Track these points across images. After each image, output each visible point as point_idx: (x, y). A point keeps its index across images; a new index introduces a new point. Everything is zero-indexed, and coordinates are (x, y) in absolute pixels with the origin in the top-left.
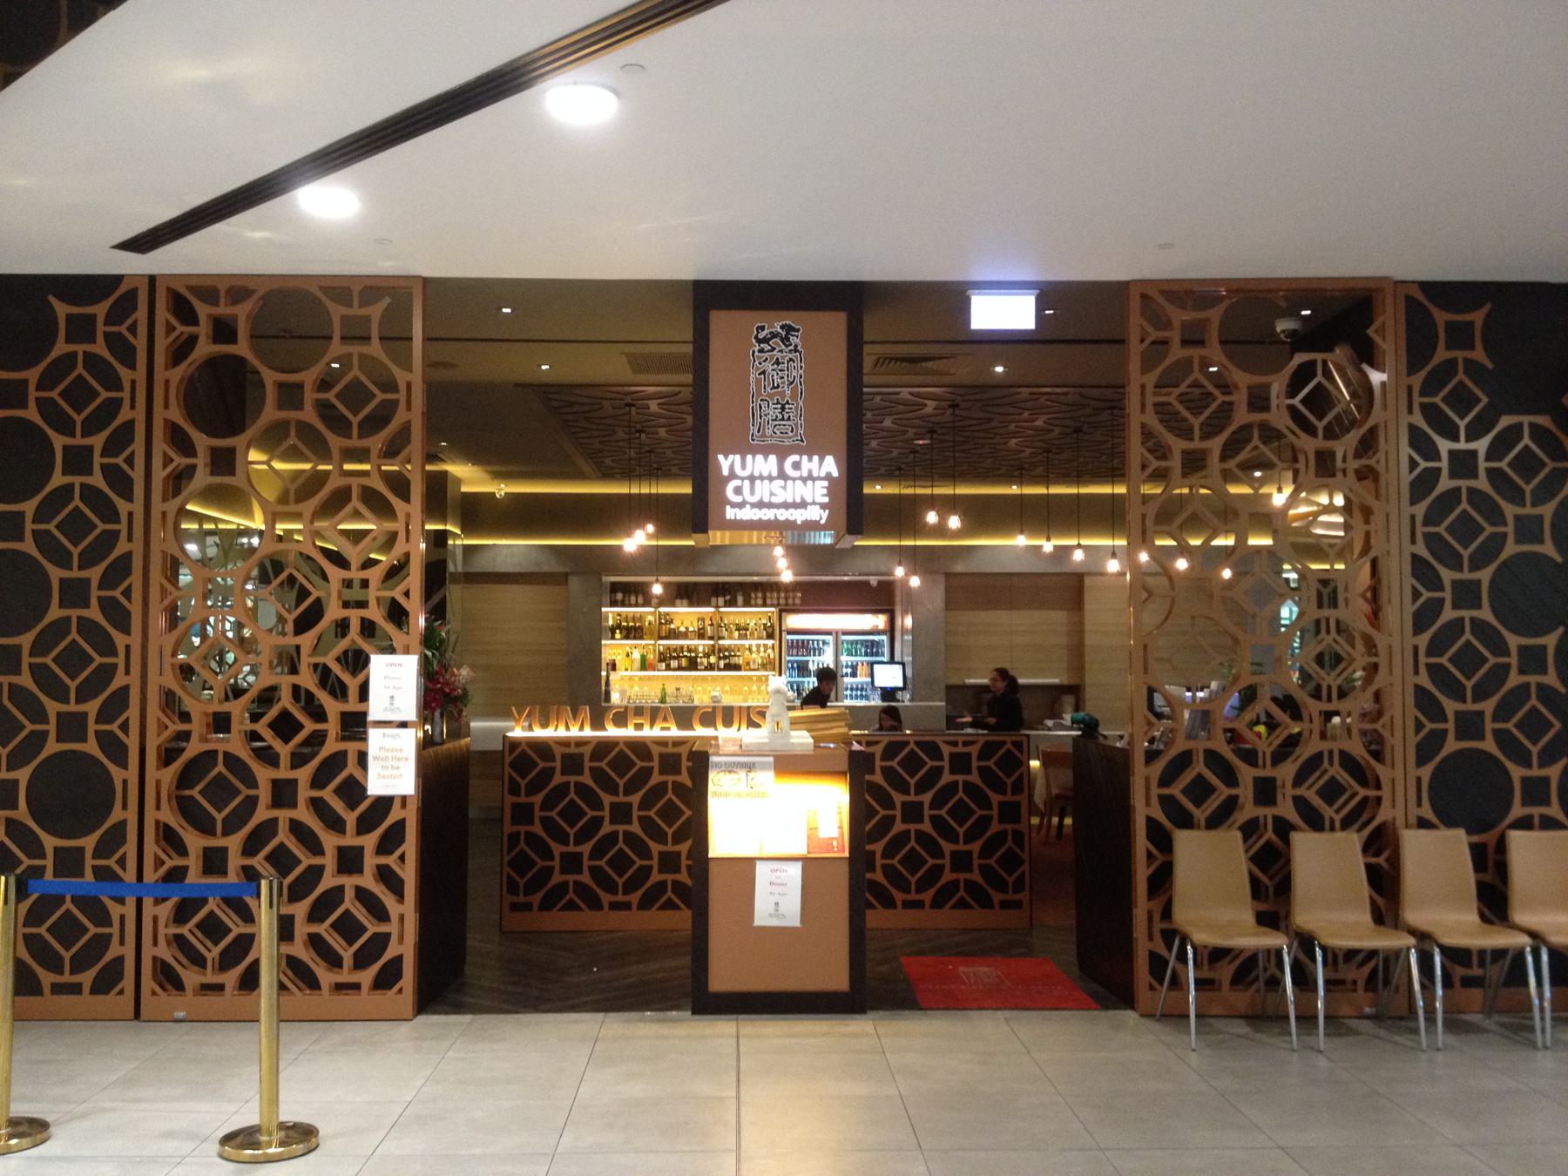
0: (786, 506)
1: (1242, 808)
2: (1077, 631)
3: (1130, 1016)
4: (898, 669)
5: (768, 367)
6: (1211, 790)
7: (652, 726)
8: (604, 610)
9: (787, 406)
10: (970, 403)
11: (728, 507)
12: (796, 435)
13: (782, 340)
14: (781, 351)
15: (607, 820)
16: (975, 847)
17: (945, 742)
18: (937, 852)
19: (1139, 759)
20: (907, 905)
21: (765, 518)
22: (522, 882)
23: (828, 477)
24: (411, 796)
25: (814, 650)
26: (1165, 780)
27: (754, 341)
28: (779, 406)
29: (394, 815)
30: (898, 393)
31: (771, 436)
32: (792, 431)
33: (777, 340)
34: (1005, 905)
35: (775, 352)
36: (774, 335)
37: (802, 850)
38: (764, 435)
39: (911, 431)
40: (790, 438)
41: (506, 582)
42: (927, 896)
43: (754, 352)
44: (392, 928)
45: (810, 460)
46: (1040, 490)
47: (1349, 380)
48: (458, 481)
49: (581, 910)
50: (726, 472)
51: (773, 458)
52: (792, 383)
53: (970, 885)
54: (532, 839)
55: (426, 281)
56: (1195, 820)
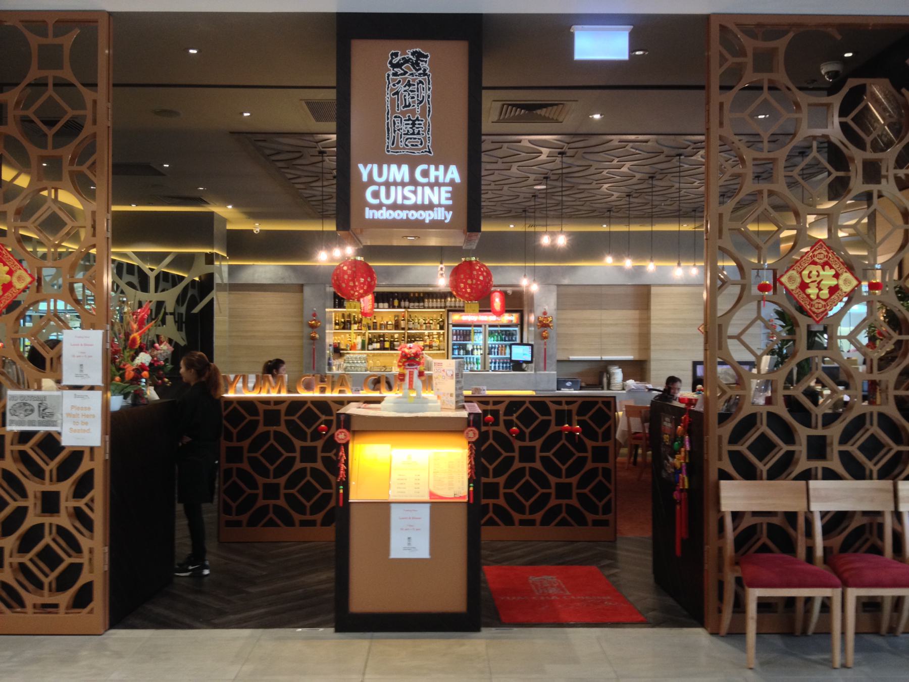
0: (416, 207)
1: (797, 463)
2: (644, 325)
3: (699, 636)
4: (527, 349)
5: (401, 88)
6: (771, 446)
7: (332, 390)
8: (327, 310)
9: (417, 122)
10: (584, 202)
11: (367, 209)
12: (424, 147)
13: (413, 64)
14: (412, 74)
15: (298, 459)
16: (574, 480)
17: (552, 402)
18: (545, 484)
19: (713, 419)
20: (523, 523)
21: (398, 218)
22: (234, 505)
23: (452, 183)
24: (98, 447)
25: (460, 334)
26: (736, 437)
27: (389, 65)
28: (410, 122)
29: (85, 466)
30: (520, 141)
31: (404, 148)
32: (421, 144)
33: (409, 65)
34: (596, 523)
35: (407, 76)
36: (406, 61)
37: (427, 498)
38: (397, 147)
39: (532, 177)
40: (420, 149)
41: (265, 291)
42: (538, 516)
43: (389, 75)
44: (84, 559)
45: (437, 169)
46: (623, 228)
47: (885, 109)
48: (224, 221)
49: (279, 526)
50: (365, 178)
51: (405, 168)
52: (421, 102)
53: (570, 509)
54: (241, 473)
55: (110, 14)
56: (758, 473)
